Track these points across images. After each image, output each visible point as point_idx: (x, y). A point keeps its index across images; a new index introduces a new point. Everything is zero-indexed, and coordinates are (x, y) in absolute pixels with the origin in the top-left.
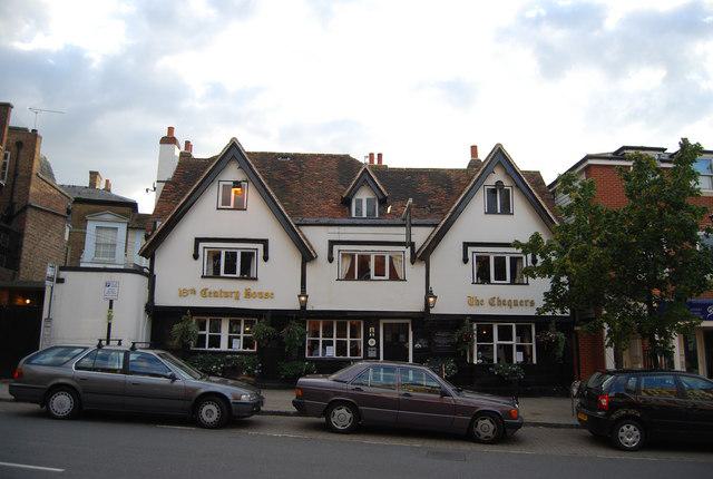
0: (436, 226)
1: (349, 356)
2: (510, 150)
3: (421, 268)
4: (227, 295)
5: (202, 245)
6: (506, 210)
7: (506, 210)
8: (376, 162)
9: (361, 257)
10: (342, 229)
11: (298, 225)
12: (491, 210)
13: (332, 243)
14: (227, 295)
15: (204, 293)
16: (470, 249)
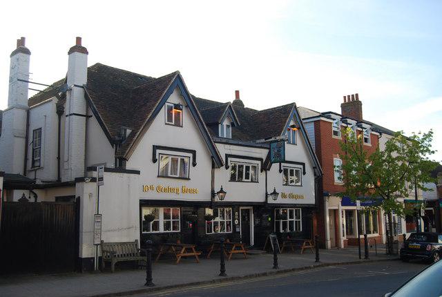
2: (82, 40)
11: (215, 142)
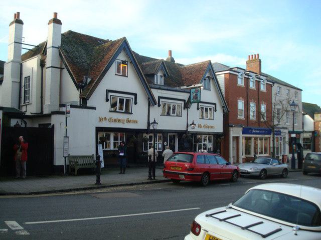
11: (151, 88)
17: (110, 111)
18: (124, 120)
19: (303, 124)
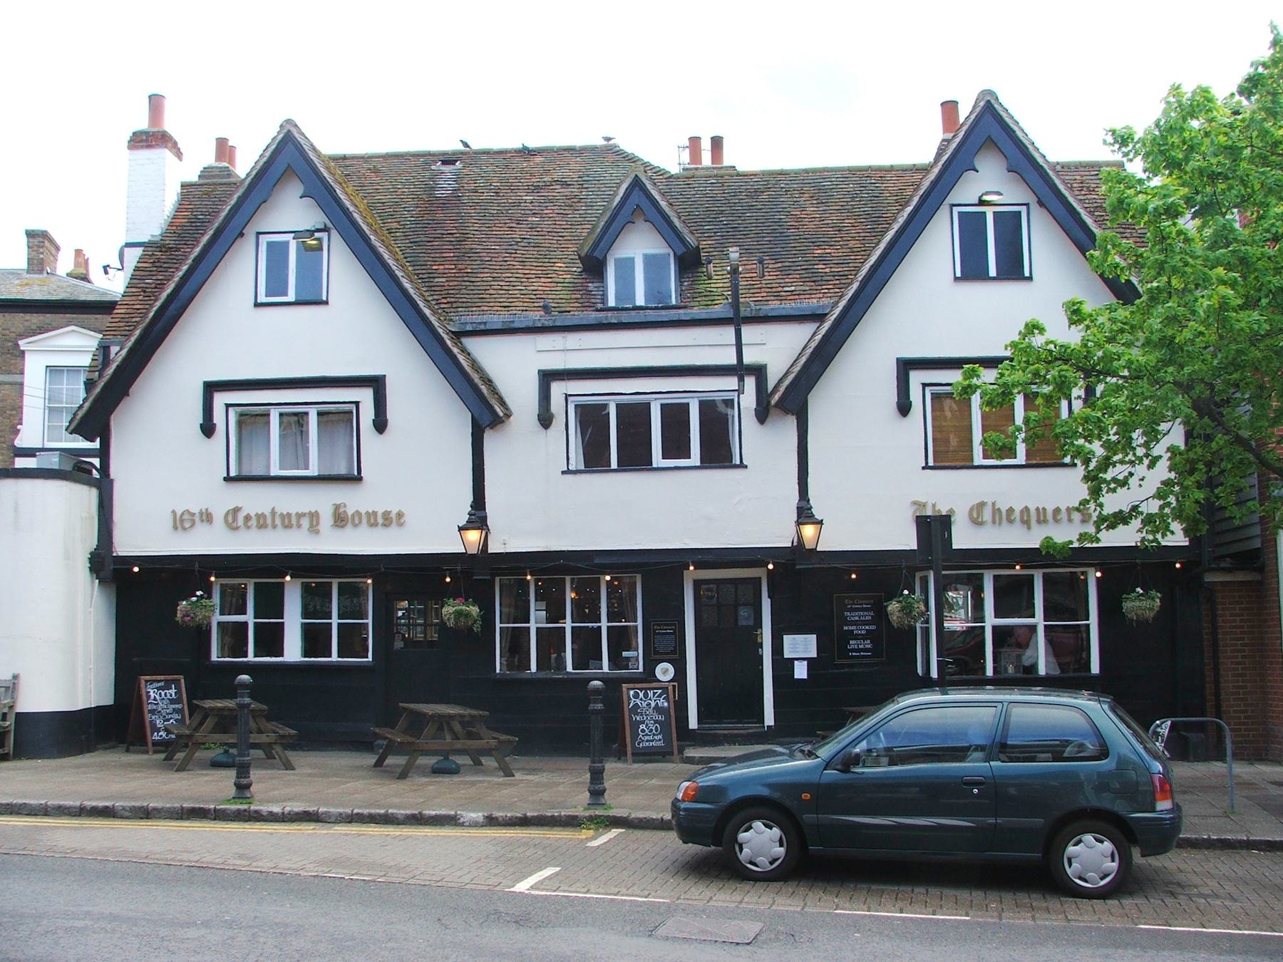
0: (818, 317)
1: (335, 657)
3: (787, 429)
4: (288, 522)
5: (220, 399)
6: (1013, 269)
7: (1013, 269)
8: (706, 159)
9: (708, 408)
10: (573, 340)
11: (458, 335)
12: (972, 270)
13: (547, 377)
14: (288, 522)
15: (233, 519)
16: (558, 389)
17: (228, 479)
18: (314, 517)
19: (16, 510)
